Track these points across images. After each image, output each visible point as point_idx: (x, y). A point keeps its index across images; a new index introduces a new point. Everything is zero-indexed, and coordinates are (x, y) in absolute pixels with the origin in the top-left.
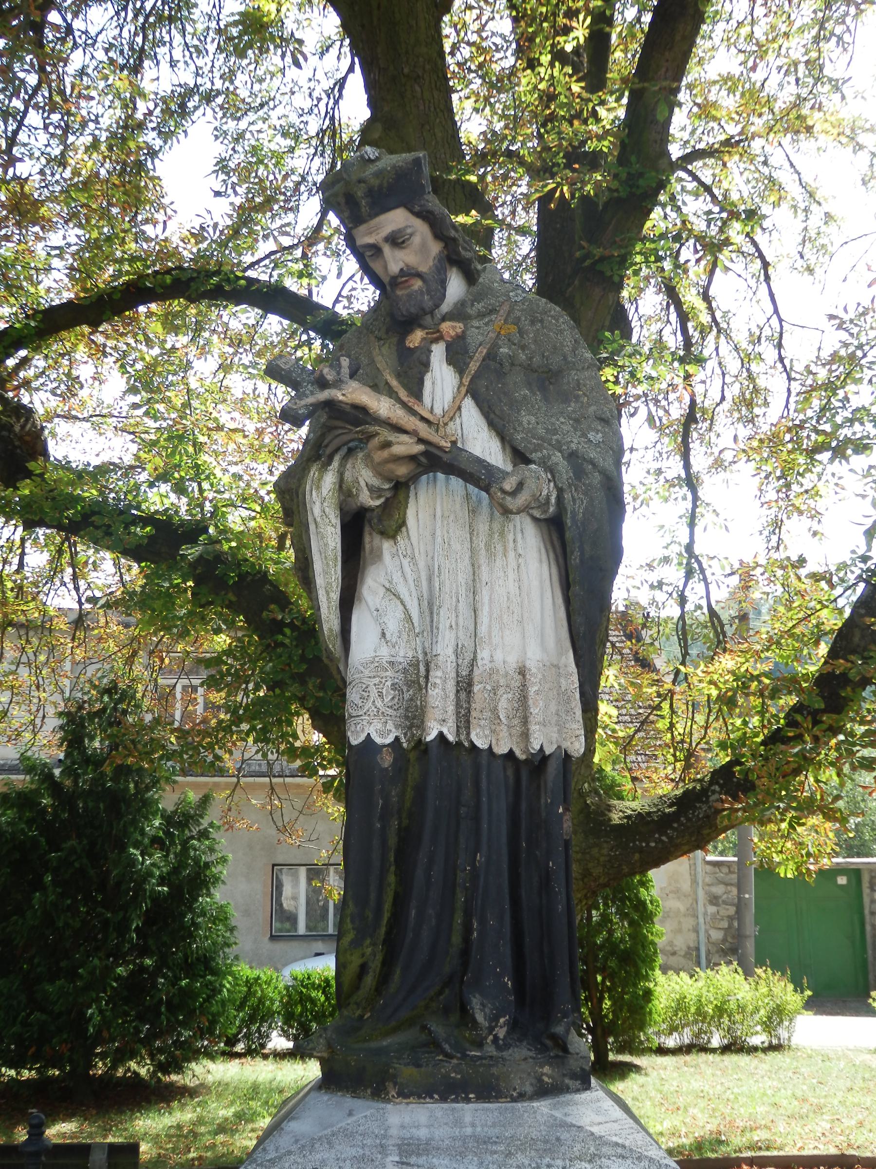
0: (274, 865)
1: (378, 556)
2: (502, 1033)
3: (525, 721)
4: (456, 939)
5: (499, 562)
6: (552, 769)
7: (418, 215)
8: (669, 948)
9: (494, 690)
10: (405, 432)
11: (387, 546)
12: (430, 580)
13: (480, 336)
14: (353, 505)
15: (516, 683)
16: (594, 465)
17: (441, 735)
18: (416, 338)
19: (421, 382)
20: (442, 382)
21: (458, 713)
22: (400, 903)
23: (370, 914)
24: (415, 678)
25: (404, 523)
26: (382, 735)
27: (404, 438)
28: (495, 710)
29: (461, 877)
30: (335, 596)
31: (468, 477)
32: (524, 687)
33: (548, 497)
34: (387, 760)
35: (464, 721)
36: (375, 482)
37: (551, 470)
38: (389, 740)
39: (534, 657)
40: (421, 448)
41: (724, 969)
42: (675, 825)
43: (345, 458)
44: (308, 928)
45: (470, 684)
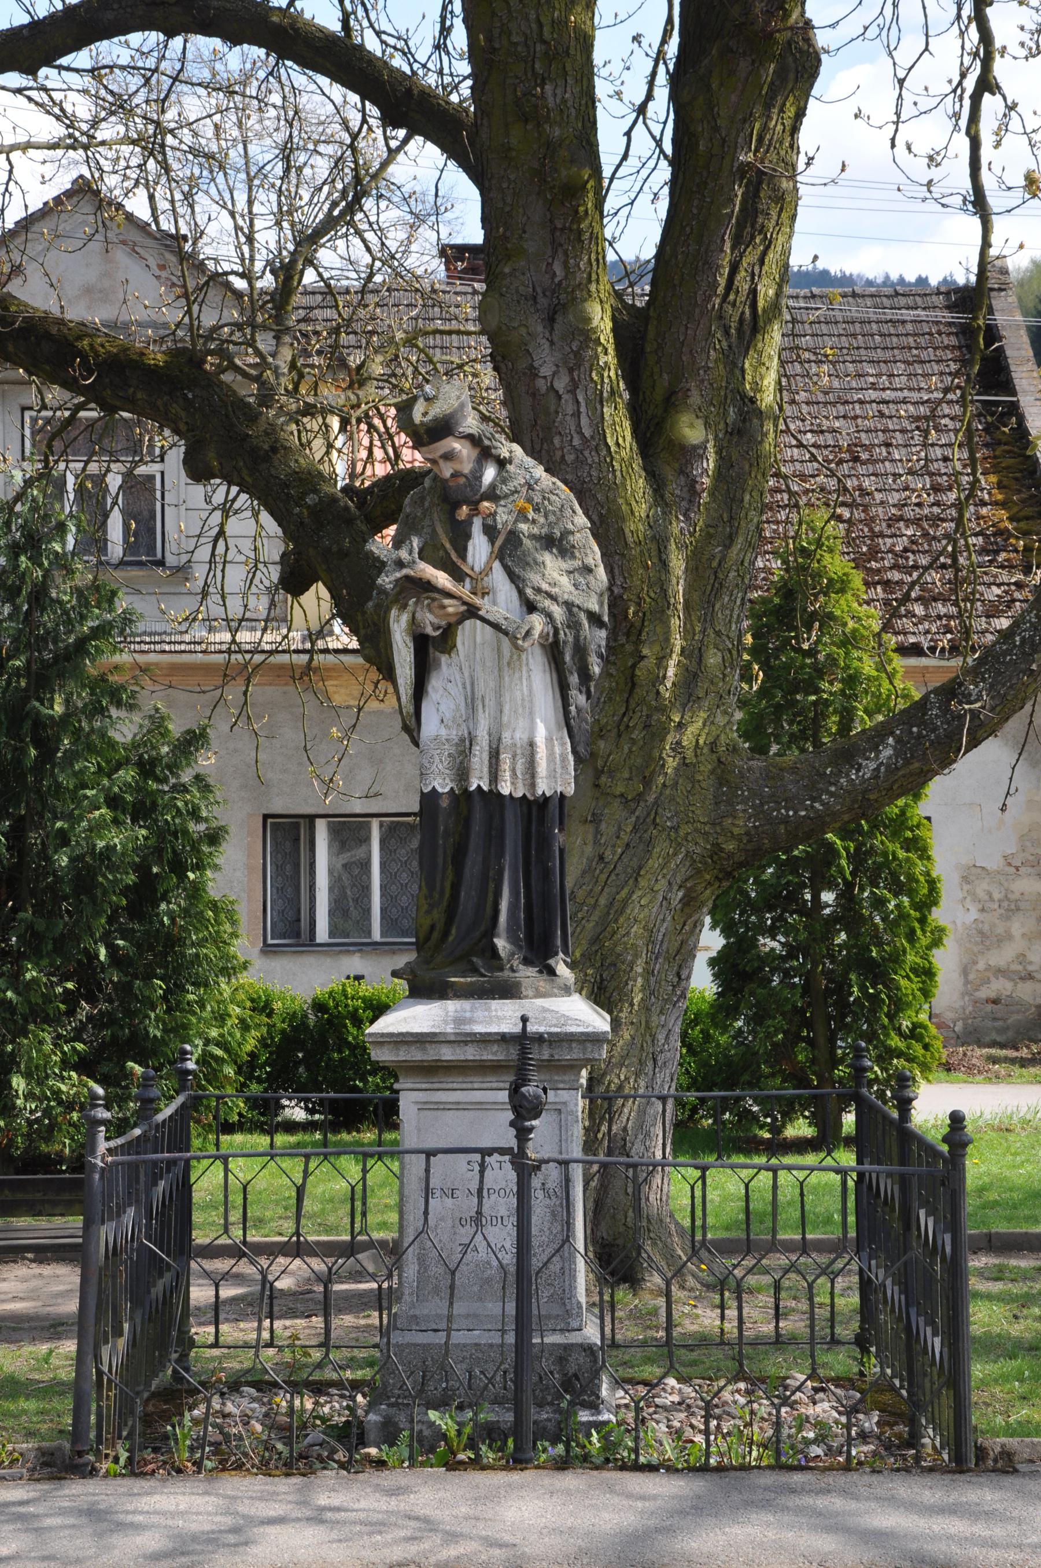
0: (266, 817)
1: (438, 665)
6: (553, 808)
8: (1016, 967)
11: (444, 659)
12: (472, 684)
14: (419, 631)
19: (465, 549)
22: (456, 887)
23: (436, 896)
24: (465, 747)
29: (491, 873)
30: (410, 692)
34: (444, 803)
35: (494, 776)
40: (464, 608)
44: (331, 935)
45: (498, 753)
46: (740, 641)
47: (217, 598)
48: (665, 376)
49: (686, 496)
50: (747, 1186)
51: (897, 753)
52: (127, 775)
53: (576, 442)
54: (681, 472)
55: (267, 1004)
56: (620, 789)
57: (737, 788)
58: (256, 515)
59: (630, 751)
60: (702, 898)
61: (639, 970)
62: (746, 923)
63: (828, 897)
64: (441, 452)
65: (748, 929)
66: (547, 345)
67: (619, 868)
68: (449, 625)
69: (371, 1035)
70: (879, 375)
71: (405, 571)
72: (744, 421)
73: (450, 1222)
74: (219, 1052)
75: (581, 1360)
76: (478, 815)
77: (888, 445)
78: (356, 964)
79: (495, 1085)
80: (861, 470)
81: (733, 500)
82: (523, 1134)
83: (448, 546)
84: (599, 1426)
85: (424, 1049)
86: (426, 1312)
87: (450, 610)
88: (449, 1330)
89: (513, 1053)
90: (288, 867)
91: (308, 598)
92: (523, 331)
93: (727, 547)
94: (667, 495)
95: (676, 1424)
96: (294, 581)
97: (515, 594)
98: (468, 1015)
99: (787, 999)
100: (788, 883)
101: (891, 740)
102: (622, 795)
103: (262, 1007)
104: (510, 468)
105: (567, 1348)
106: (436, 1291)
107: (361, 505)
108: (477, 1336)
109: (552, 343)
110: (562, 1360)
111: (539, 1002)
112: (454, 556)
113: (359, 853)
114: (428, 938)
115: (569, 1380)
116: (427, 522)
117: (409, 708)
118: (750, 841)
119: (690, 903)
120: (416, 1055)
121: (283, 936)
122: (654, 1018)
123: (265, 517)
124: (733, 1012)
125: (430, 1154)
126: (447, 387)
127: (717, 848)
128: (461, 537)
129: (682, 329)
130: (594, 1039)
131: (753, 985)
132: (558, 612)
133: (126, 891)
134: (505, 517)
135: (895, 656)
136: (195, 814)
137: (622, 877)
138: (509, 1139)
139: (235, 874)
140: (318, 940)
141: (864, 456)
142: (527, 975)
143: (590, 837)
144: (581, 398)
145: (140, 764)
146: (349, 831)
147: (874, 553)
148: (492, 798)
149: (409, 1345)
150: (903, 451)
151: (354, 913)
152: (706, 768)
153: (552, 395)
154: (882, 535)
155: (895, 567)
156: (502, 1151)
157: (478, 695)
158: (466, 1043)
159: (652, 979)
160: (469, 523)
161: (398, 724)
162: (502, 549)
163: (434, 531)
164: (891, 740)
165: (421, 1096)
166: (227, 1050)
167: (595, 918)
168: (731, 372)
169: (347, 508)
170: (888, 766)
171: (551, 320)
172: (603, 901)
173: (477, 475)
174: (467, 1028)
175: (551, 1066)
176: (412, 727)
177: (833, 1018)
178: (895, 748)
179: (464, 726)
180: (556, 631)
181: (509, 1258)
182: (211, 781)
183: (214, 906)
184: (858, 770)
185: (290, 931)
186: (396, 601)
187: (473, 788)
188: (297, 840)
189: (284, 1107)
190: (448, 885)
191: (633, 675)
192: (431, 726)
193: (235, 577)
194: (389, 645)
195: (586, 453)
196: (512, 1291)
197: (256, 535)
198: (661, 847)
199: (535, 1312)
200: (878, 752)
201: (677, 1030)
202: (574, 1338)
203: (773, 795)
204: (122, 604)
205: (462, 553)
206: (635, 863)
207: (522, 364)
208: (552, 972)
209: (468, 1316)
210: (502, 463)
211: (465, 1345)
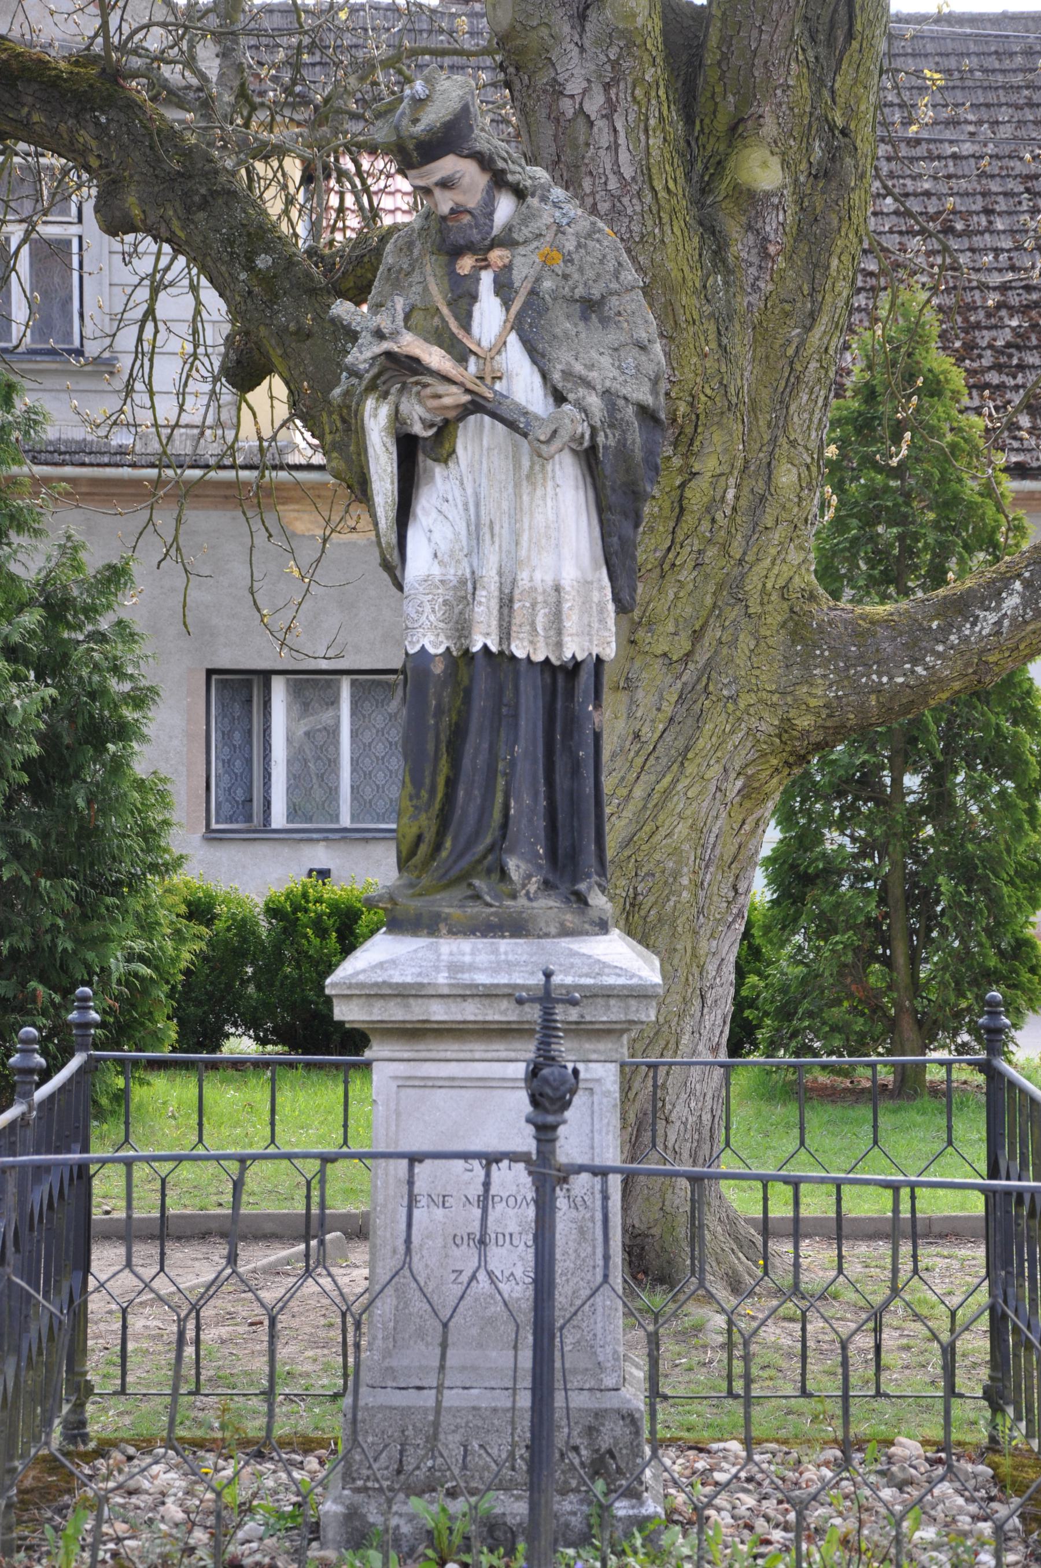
0: (210, 672)
1: (432, 478)
2: (532, 888)
3: (559, 632)
4: (497, 815)
5: (539, 492)
6: (585, 677)
7: (466, 157)
9: (533, 605)
10: (454, 383)
11: (438, 470)
12: (477, 505)
13: (523, 272)
15: (552, 600)
16: (626, 399)
17: (485, 647)
18: (466, 264)
19: (469, 315)
20: (489, 316)
21: (500, 626)
22: (451, 783)
23: (424, 794)
25: (454, 451)
26: (435, 647)
27: (454, 389)
28: (533, 624)
29: (501, 766)
30: (392, 514)
31: (511, 425)
32: (559, 604)
33: (582, 436)
36: (427, 416)
37: (584, 410)
38: (441, 650)
39: (569, 576)
40: (467, 398)
41: (140, 768)
42: (940, 648)
43: (401, 391)
44: (293, 812)
45: (511, 601)
46: (821, 452)
47: (145, 399)
48: (731, 98)
49: (755, 259)
50: (802, 1143)
51: (1026, 603)
52: (31, 618)
53: (613, 184)
54: (749, 228)
55: (210, 906)
56: (662, 647)
57: (816, 646)
58: (194, 288)
59: (677, 597)
60: (767, 788)
61: (685, 881)
62: (808, 814)
63: (912, 781)
64: (437, 177)
65: (811, 820)
66: (575, 52)
67: (660, 749)
68: (446, 422)
69: (334, 985)
70: (980, 123)
71: (386, 346)
72: (833, 160)
73: (440, 1242)
74: (145, 971)
75: (618, 1432)
76: (482, 686)
77: (988, 212)
78: (320, 856)
79: (503, 1055)
80: (954, 244)
81: (816, 266)
82: (158, 24)
83: (445, 311)
84: (641, 1522)
85: (407, 1006)
86: (406, 1362)
87: (447, 401)
88: (440, 1388)
89: (533, 1013)
90: (237, 735)
91: (258, 396)
92: (544, 32)
93: (808, 329)
94: (731, 260)
95: (742, 1511)
96: (243, 372)
97: (537, 379)
98: (467, 959)
99: (859, 909)
100: (863, 764)
101: (1018, 585)
102: (665, 655)
103: (200, 911)
104: (534, 202)
105: (599, 1414)
106: (421, 1334)
107: (330, 269)
108: (475, 1397)
109: (582, 49)
110: (591, 1431)
111: (565, 943)
112: (454, 326)
113: (326, 717)
114: (413, 853)
115: (602, 1459)
116: (416, 277)
117: (390, 537)
118: (830, 716)
119: (752, 794)
120: (394, 1013)
121: (230, 820)
122: (703, 944)
123: (210, 295)
124: (789, 924)
125: (414, 1159)
126: (447, 84)
127: (786, 726)
128: (464, 298)
129: (755, 33)
130: (639, 994)
131: (817, 892)
132: (594, 401)
133: (28, 765)
134: (525, 271)
135: (1003, 477)
136: (117, 670)
137: (664, 761)
138: (525, 1141)
139: (168, 746)
140: (275, 825)
141: (959, 226)
142: (547, 907)
143: (623, 709)
144: (619, 126)
145: (47, 606)
146: (313, 685)
147: (970, 347)
148: (500, 661)
149: (382, 1408)
150: (1007, 220)
151: (318, 794)
152: (774, 619)
153: (581, 120)
154: (978, 326)
155: (998, 367)
156: (514, 1157)
157: (485, 520)
158: (464, 997)
159: (701, 894)
160: (474, 278)
161: (375, 558)
162: (520, 316)
163: (426, 289)
164: (1018, 585)
165: (400, 1069)
166: (156, 969)
167: (627, 814)
168: (818, 92)
169: (308, 275)
170: (1013, 619)
171: (582, 17)
172: (638, 792)
173: (488, 209)
174: (466, 978)
175: (582, 1030)
176: (393, 565)
177: (916, 932)
178: (1023, 596)
179: (465, 563)
180: (594, 430)
181: (519, 1290)
182: (136, 628)
183: (140, 785)
184: (974, 624)
185: (239, 814)
186: (372, 387)
187: (476, 648)
188: (249, 701)
189: (227, 1036)
190: (441, 781)
191: (681, 498)
192: (420, 561)
193: (167, 372)
194: (362, 449)
195: (626, 200)
196: (528, 1338)
197: (196, 312)
198: (716, 721)
199: (558, 1364)
200: (1000, 601)
201: (732, 958)
202: (610, 1401)
203: (861, 656)
204: (22, 403)
205: (466, 321)
206: (681, 743)
207: (542, 79)
208: (581, 899)
209: (464, 1368)
210: (520, 193)
211: (459, 1410)
